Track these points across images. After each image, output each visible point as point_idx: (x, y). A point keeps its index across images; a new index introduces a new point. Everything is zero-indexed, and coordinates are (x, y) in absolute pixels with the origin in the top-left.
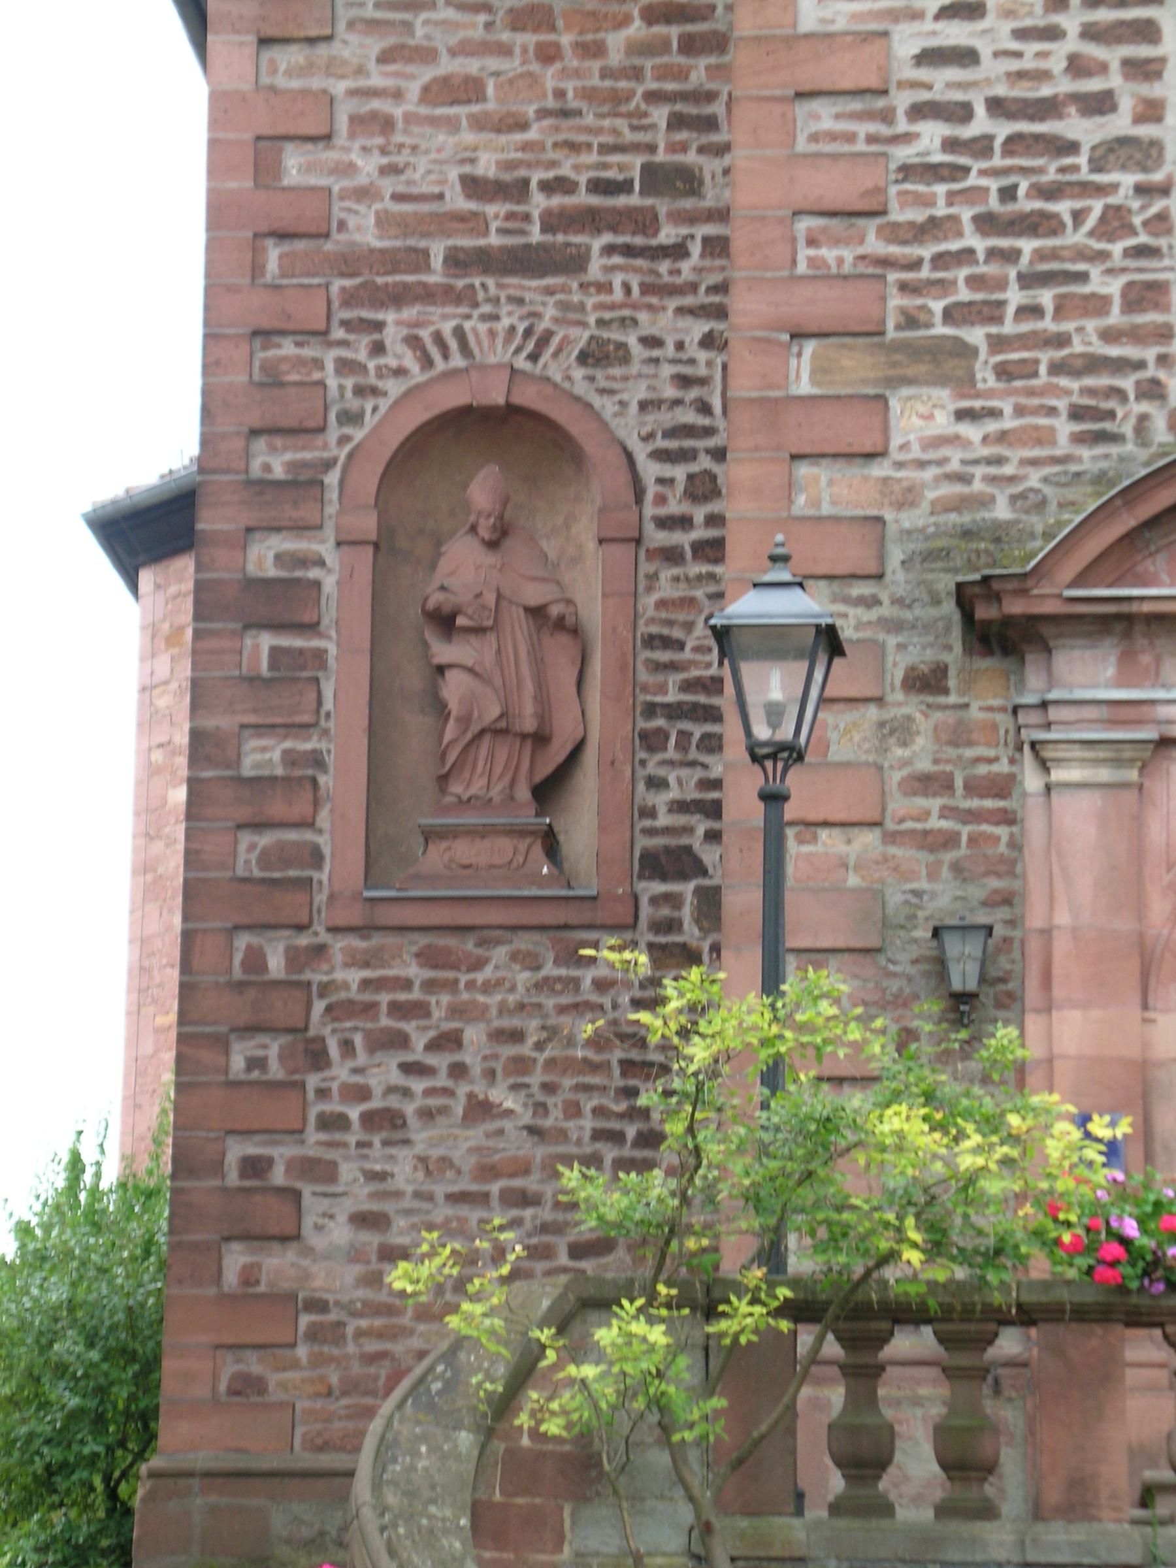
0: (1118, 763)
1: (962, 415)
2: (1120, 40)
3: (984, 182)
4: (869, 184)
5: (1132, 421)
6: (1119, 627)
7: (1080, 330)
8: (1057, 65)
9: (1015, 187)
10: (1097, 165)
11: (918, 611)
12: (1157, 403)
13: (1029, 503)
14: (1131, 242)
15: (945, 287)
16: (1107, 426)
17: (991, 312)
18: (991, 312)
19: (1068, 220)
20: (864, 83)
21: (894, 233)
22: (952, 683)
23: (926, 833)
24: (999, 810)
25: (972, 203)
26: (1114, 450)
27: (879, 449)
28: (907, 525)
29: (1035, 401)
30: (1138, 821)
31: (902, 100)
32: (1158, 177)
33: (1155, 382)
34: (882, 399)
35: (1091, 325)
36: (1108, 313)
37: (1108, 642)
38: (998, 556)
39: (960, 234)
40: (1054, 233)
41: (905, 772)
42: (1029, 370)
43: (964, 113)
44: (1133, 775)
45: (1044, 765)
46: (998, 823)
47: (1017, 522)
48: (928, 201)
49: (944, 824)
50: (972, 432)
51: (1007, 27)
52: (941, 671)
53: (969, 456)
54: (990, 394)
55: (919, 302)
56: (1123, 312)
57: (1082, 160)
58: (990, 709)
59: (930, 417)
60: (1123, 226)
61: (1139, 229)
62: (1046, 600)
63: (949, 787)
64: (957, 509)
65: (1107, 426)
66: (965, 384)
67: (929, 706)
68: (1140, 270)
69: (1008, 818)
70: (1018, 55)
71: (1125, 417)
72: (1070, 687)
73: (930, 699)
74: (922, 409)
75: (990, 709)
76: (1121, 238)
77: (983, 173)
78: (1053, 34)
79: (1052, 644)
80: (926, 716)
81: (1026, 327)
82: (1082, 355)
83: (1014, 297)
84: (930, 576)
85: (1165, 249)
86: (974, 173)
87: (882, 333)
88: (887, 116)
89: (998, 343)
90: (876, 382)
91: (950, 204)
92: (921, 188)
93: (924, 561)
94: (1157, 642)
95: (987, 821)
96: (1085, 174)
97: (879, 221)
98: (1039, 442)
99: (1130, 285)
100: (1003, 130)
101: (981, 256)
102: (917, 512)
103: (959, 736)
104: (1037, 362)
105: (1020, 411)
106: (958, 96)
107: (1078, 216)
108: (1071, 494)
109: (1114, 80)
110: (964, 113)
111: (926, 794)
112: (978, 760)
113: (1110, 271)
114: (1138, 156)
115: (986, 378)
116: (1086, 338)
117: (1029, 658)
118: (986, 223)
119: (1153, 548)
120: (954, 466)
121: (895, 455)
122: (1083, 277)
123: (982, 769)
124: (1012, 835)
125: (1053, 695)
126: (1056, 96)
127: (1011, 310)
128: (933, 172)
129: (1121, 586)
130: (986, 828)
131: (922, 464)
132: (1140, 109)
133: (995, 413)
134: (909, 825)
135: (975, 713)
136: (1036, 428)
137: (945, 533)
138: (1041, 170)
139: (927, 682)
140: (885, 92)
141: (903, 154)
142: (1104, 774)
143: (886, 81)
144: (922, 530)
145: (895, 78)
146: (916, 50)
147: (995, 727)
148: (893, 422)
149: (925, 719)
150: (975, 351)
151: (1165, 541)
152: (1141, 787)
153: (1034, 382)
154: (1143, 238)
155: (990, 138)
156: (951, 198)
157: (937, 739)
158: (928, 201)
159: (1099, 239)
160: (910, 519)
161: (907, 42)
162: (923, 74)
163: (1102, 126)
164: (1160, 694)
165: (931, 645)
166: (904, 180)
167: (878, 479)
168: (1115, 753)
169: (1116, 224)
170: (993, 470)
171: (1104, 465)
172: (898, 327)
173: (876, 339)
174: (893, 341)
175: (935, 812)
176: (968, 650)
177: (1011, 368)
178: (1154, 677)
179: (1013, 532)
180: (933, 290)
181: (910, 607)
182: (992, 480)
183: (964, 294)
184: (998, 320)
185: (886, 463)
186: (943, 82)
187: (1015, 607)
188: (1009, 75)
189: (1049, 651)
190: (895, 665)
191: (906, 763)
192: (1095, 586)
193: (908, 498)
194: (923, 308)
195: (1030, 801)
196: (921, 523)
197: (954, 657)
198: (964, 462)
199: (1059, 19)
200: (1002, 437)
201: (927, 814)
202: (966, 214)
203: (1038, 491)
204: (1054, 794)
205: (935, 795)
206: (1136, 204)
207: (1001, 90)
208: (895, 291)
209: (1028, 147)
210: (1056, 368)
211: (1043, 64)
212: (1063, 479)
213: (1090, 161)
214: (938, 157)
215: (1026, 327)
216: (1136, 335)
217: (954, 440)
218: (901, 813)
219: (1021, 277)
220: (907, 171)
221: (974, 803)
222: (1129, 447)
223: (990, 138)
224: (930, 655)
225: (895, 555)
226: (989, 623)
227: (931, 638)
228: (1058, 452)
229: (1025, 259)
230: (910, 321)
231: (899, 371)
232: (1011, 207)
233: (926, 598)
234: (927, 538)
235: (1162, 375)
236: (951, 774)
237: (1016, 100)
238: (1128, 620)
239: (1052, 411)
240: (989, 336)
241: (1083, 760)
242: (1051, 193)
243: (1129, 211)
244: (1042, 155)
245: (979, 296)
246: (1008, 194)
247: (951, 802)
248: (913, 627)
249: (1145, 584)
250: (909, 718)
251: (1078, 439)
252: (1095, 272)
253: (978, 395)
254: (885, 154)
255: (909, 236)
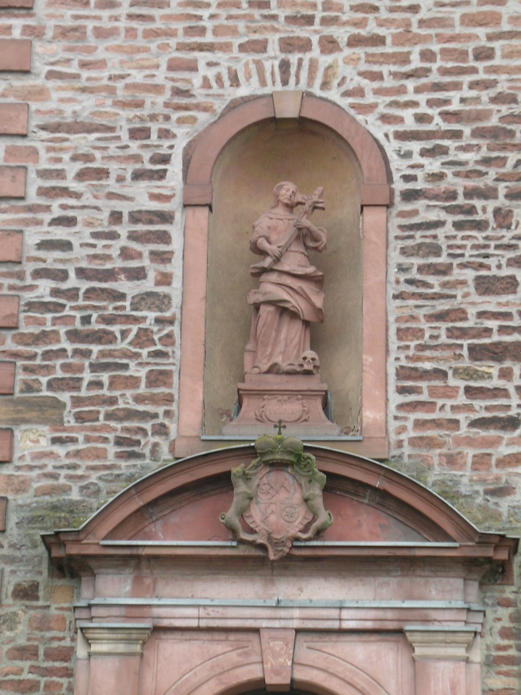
0: (129, 641)
1: (55, 441)
2: (148, 241)
3: (73, 313)
4: (8, 312)
5: (150, 447)
6: (133, 562)
7: (123, 395)
8: (115, 252)
9: (90, 316)
10: (135, 308)
11: (24, 552)
12: (164, 437)
13: (90, 491)
14: (153, 349)
15: (49, 369)
16: (136, 449)
17: (74, 384)
18: (74, 384)
19: (118, 336)
20: (8, 258)
21: (22, 339)
22: (41, 594)
23: (20, 682)
24: (63, 668)
25: (66, 324)
26: (139, 462)
27: (6, 459)
28: (20, 502)
29: (97, 434)
30: (139, 675)
31: (29, 268)
32: (168, 314)
33: (163, 426)
34: (10, 431)
35: (129, 393)
36: (138, 387)
37: (128, 571)
38: (71, 521)
39: (58, 341)
40: (111, 342)
41: (10, 646)
42: (94, 416)
43: (63, 275)
44: (138, 648)
45: (88, 642)
46: (62, 676)
47: (83, 501)
48: (42, 323)
49: (31, 677)
50: (60, 450)
51: (88, 231)
52: (35, 586)
53: (58, 464)
54: (72, 429)
55: (34, 377)
56: (147, 387)
57: (127, 304)
58: (62, 609)
59: (37, 441)
60: (148, 340)
61: (157, 342)
62: (91, 545)
63: (35, 654)
64: (49, 494)
65: (136, 449)
66: (58, 423)
67: (27, 607)
68: (157, 364)
69: (69, 673)
70: (94, 246)
71: (146, 444)
72: (105, 596)
73: (28, 603)
74: (33, 437)
75: (62, 609)
76: (147, 346)
77: (73, 308)
78: (113, 236)
79: (96, 571)
80: (25, 612)
81: (93, 393)
82: (124, 409)
83: (87, 376)
84: (32, 532)
85: (170, 353)
86: (67, 308)
87: (12, 394)
88: (20, 276)
89: (77, 401)
90: (7, 421)
91: (54, 325)
92: (38, 315)
93: (29, 523)
94: (154, 572)
95: (55, 675)
96: (128, 311)
97: (14, 332)
98: (98, 457)
99: (151, 371)
100: (84, 285)
101: (70, 353)
102: (27, 495)
103: (43, 624)
104: (98, 412)
105: (88, 439)
106: (61, 266)
107: (124, 334)
108: (113, 486)
109: (146, 262)
110: (63, 275)
111: (21, 659)
112: (53, 639)
113: (140, 364)
114: (157, 302)
115: (69, 420)
116: (126, 400)
117: (84, 579)
118: (74, 335)
119: (154, 518)
120: (49, 469)
121: (17, 462)
122: (125, 367)
123: (55, 644)
124: (70, 683)
125: (93, 602)
126: (114, 268)
127: (85, 383)
128: (45, 307)
129: (136, 539)
130: (55, 679)
131: (31, 468)
132: (159, 278)
133: (73, 440)
134: (11, 677)
135: (53, 611)
136: (96, 449)
137: (42, 508)
138: (105, 308)
139: (26, 593)
140: (20, 263)
141: (28, 296)
142: (121, 648)
143: (21, 257)
144: (28, 505)
145: (26, 255)
146: (38, 241)
147: (64, 619)
148: (16, 444)
149: (23, 614)
150: (64, 405)
151: (161, 515)
152: (142, 655)
153: (96, 424)
154: (159, 347)
155: (77, 289)
156: (55, 321)
157: (30, 626)
158: (42, 323)
159: (135, 347)
160: (23, 499)
161: (33, 237)
162: (42, 254)
163: (139, 286)
164: (155, 602)
165: (30, 571)
166: (28, 311)
167: (6, 476)
168: (127, 635)
169: (145, 338)
170: (71, 472)
171: (133, 470)
172: (22, 391)
173: (8, 397)
174: (18, 398)
175: (26, 670)
176: (51, 574)
177: (84, 415)
178: (153, 592)
179: (81, 508)
180: (42, 371)
181: (19, 549)
182: (70, 477)
183: (59, 374)
184: (78, 389)
185: (11, 466)
186: (52, 259)
187: (74, 550)
188: (88, 256)
189: (94, 575)
190: (9, 582)
191: (12, 640)
192: (121, 539)
193: (22, 487)
194: (36, 380)
195: (80, 663)
196: (28, 501)
197: (43, 579)
198: (55, 467)
199: (117, 228)
200: (77, 454)
201: (21, 671)
202: (62, 330)
203: (96, 484)
204: (92, 659)
205: (27, 659)
206: (155, 329)
207: (84, 264)
208: (20, 371)
209: (98, 295)
210: (109, 416)
211: (107, 252)
212: (110, 478)
213: (132, 304)
214: (48, 299)
215: (93, 393)
216: (153, 399)
217: (50, 455)
218: (6, 670)
219: (91, 365)
220: (31, 306)
221: (49, 664)
222: (148, 461)
223: (77, 289)
224: (29, 577)
225: (13, 519)
226: (61, 559)
227: (30, 568)
228: (108, 463)
229: (94, 356)
230: (28, 388)
231: (21, 416)
232: (87, 327)
233: (29, 544)
234: (32, 510)
235: (166, 422)
236: (37, 646)
237: (91, 270)
238: (139, 557)
239: (105, 440)
240: (72, 397)
241: (110, 639)
242: (109, 320)
243: (152, 332)
244: (105, 300)
245: (68, 375)
246: (86, 320)
247: (36, 664)
248: (21, 561)
249: (150, 539)
250: (15, 614)
251: (119, 456)
252: (132, 364)
253: (64, 430)
254: (18, 296)
255: (30, 341)
